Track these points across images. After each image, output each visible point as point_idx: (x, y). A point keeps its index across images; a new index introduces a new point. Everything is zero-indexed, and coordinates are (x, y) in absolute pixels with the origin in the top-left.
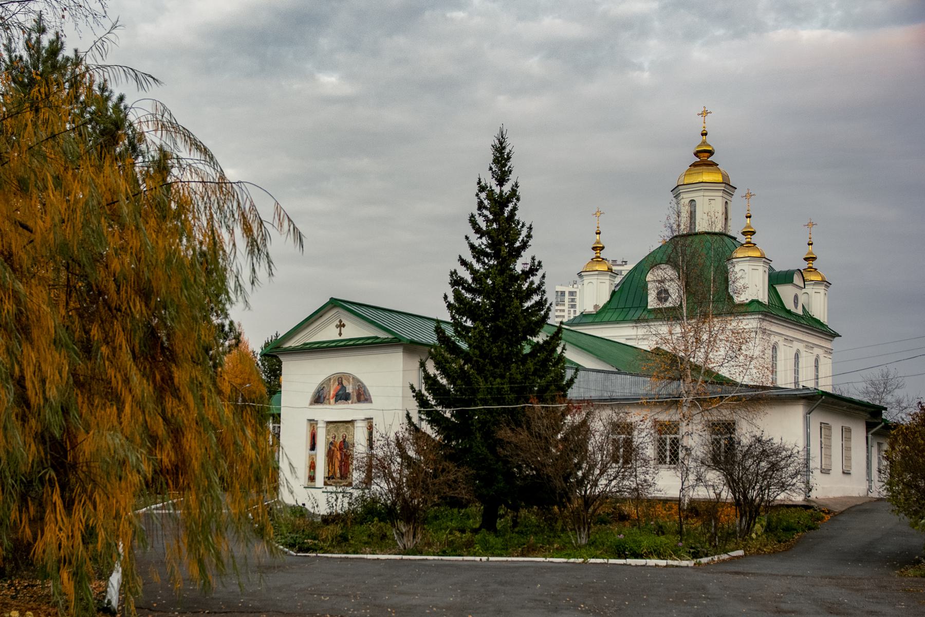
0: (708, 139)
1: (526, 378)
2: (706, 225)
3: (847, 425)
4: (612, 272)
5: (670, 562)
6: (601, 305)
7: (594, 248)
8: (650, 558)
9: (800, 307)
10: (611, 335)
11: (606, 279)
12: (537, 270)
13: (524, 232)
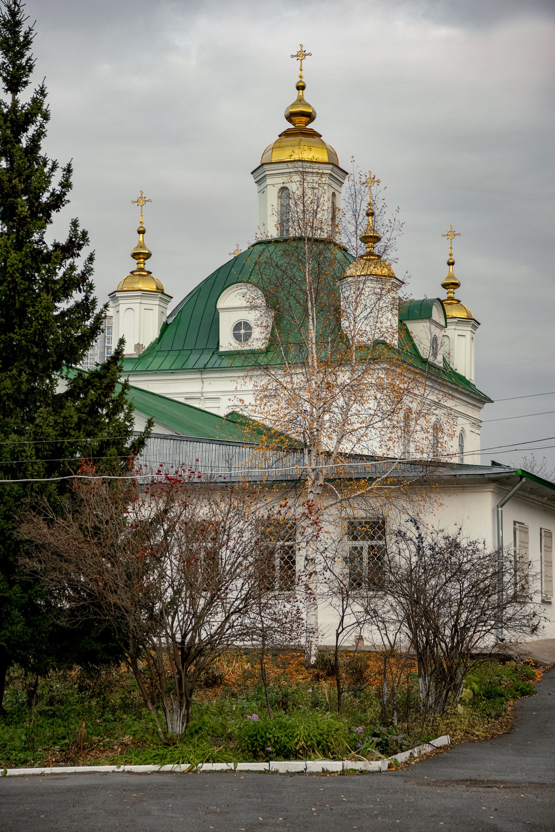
0: (307, 95)
1: (64, 434)
2: (347, 195)
3: (547, 526)
4: (163, 293)
5: (350, 765)
6: (146, 345)
7: (135, 255)
8: (310, 759)
9: (440, 358)
10: (171, 391)
11: (155, 303)
12: (80, 247)
13: (57, 178)
